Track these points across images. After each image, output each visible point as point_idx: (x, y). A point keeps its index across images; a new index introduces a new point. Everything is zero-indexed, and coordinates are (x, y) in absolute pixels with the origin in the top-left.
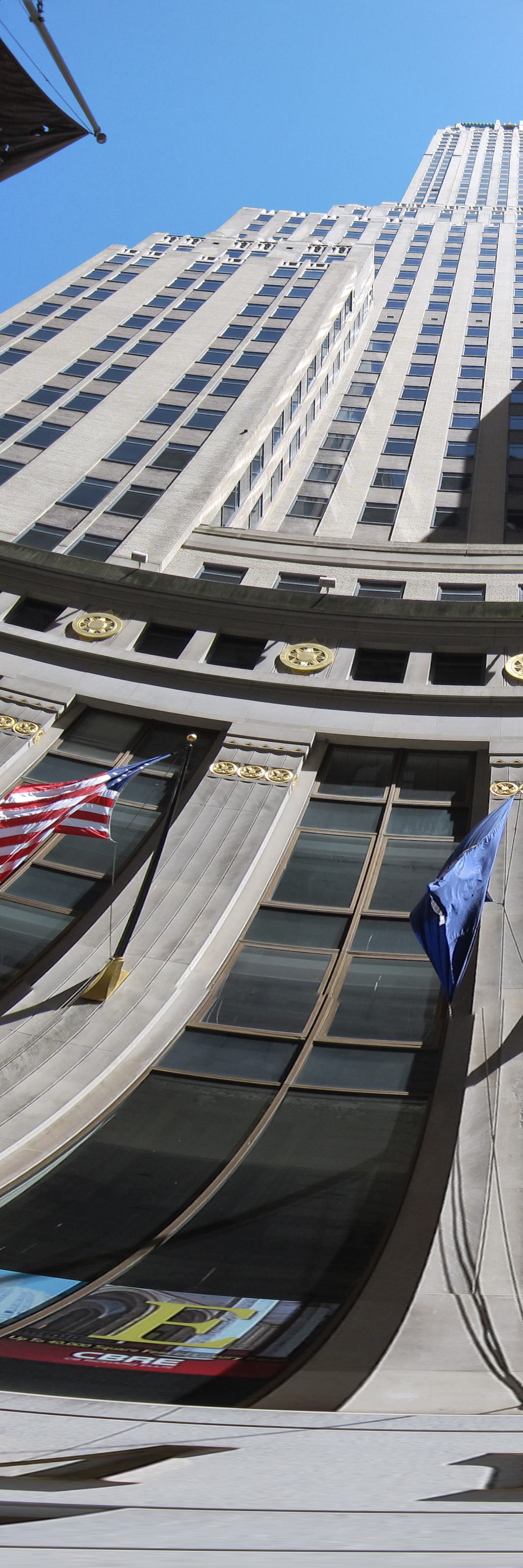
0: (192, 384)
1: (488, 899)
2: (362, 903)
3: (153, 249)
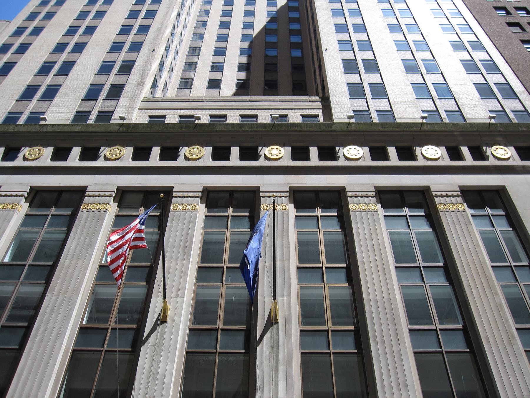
1: (261, 257)
2: (226, 263)
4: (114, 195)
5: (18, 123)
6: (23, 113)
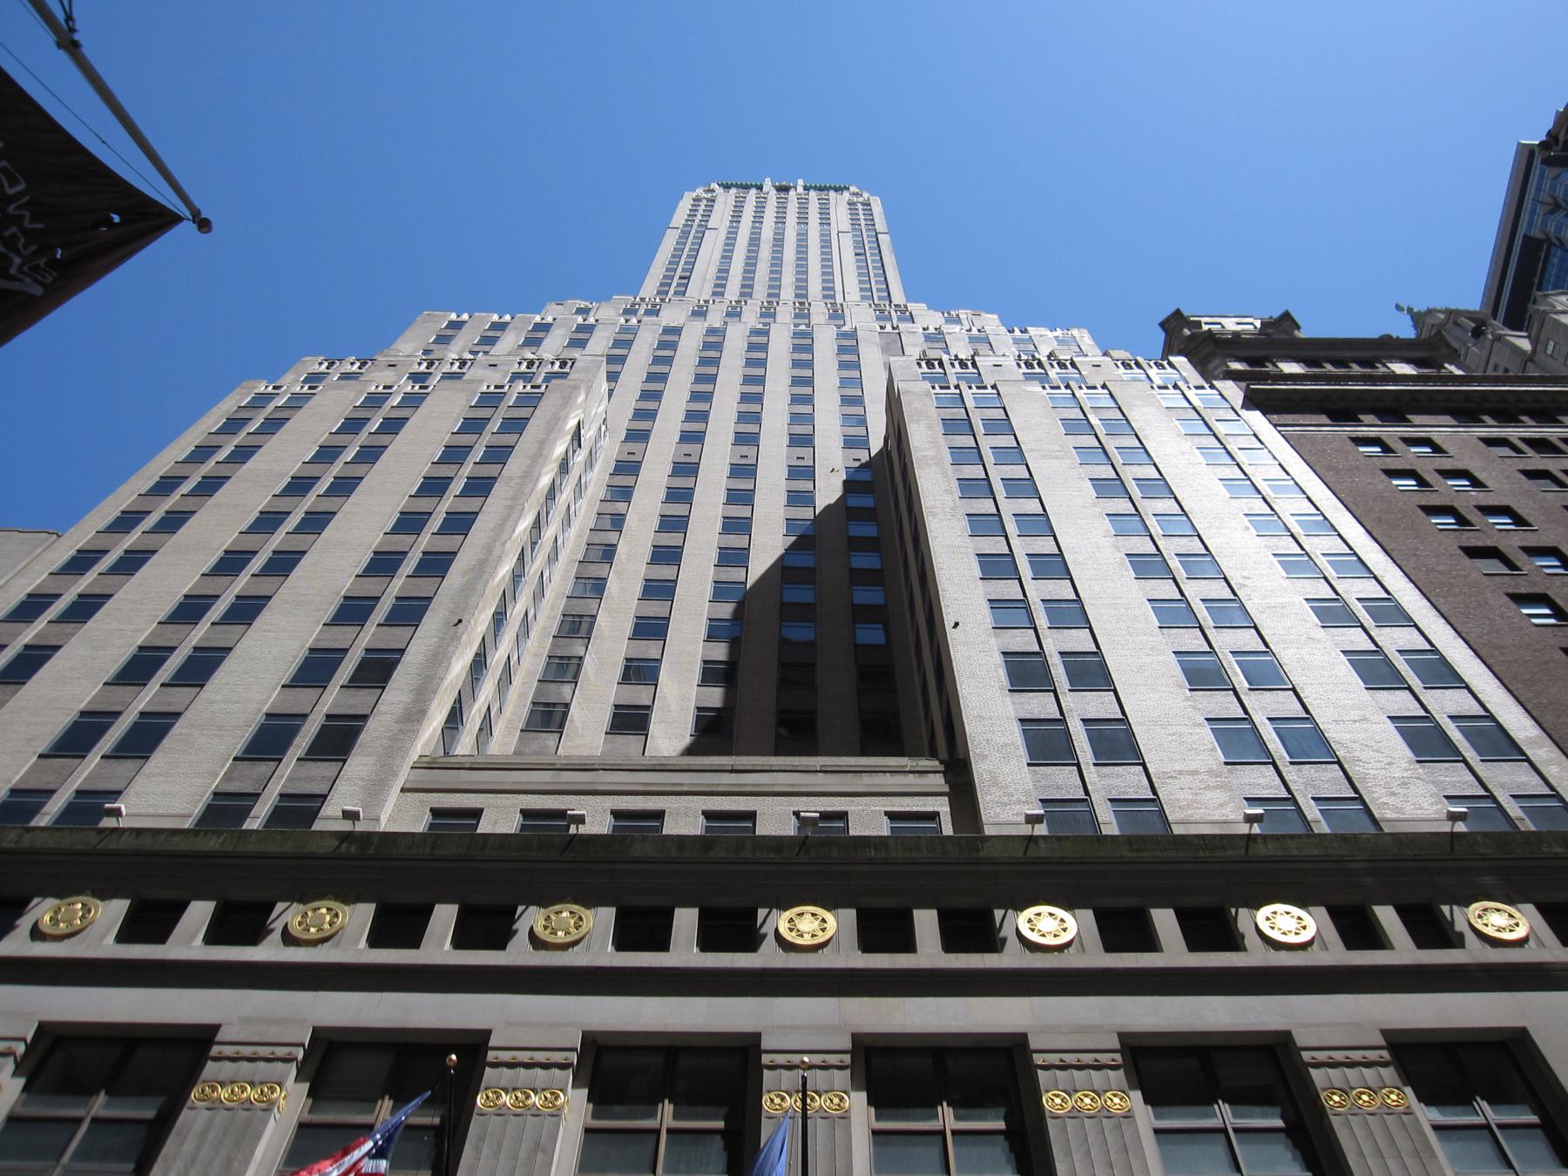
0: (383, 564)
3: (305, 381)
4: (300, 1056)
5: (33, 824)
6: (53, 792)
